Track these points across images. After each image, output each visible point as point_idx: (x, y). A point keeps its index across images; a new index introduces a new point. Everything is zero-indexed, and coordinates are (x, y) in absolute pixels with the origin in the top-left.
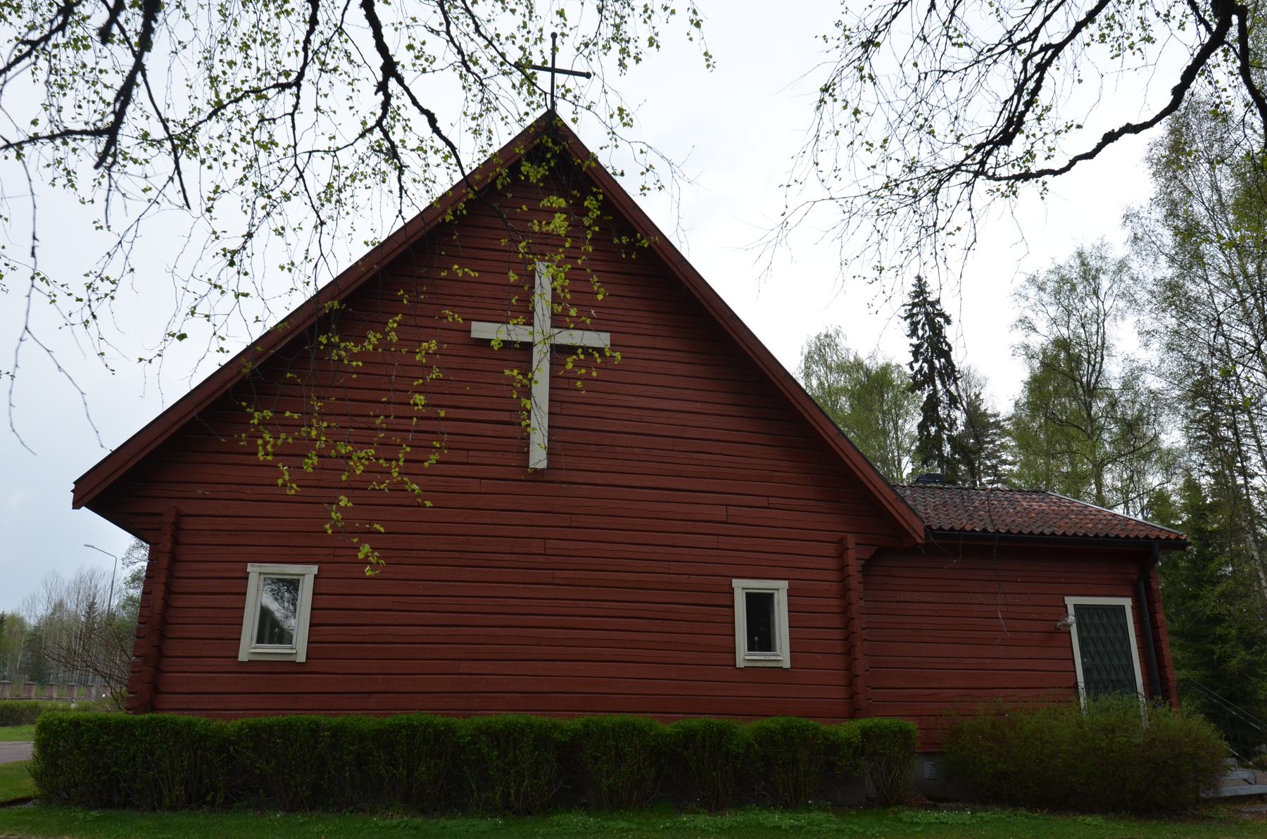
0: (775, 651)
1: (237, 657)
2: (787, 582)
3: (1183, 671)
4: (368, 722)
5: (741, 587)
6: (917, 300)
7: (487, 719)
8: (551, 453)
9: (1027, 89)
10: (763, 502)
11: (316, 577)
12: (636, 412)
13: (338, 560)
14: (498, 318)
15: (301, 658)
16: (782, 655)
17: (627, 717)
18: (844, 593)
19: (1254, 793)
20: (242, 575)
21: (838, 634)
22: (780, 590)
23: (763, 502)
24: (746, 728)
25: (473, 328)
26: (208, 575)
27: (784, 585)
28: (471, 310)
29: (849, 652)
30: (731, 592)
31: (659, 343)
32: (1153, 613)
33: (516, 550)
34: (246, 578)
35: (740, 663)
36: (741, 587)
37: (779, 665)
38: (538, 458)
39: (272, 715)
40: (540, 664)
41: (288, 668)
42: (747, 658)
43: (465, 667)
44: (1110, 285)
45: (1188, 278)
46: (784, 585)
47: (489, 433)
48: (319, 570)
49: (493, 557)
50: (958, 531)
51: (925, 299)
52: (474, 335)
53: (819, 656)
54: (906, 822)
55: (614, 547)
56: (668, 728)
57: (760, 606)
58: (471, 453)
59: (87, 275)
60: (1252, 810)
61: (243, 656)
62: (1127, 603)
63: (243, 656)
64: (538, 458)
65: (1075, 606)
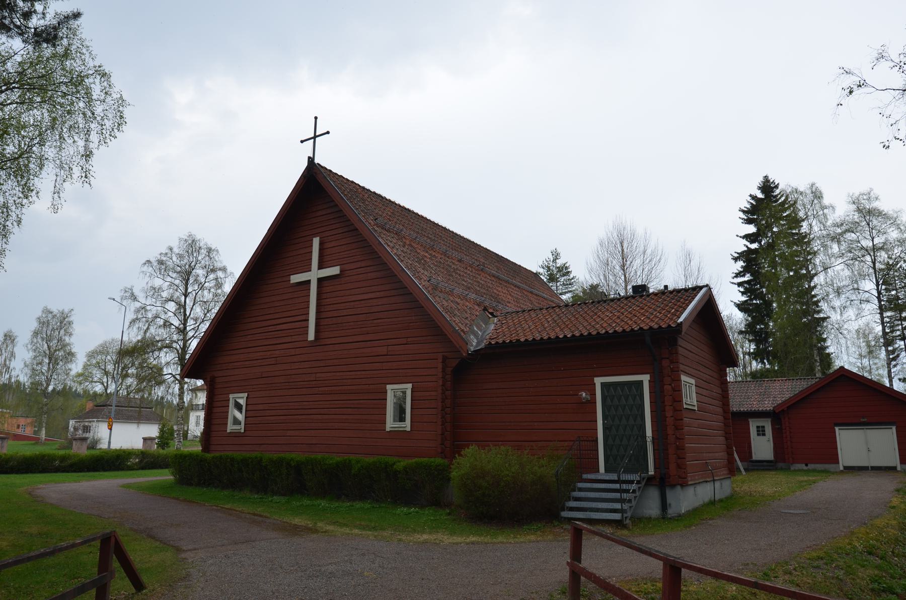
0: (405, 421)
2: (411, 384)
3: (72, 429)
11: (247, 398)
13: (254, 390)
14: (305, 270)
15: (408, 429)
16: (407, 425)
17: (417, 459)
19: (605, 518)
24: (401, 464)
31: (363, 264)
34: (386, 392)
37: (405, 429)
38: (311, 336)
39: (276, 453)
43: (289, 433)
46: (410, 386)
47: (299, 327)
50: (621, 333)
53: (425, 424)
54: (368, 509)
55: (367, 372)
56: (367, 460)
58: (293, 337)
61: (388, 429)
62: (645, 378)
63: (388, 429)
65: (642, 381)
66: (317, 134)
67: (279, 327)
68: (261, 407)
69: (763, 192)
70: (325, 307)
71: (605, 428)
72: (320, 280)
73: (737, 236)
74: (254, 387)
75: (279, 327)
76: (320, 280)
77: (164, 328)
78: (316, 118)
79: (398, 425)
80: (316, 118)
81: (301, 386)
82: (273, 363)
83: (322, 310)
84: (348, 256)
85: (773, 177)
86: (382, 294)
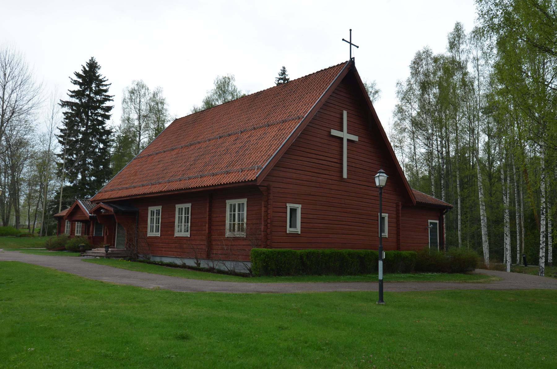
1: (286, 232)
4: (327, 251)
5: (289, 206)
6: (281, 77)
7: (279, 250)
8: (342, 115)
12: (361, 162)
13: (305, 203)
16: (298, 229)
20: (285, 207)
22: (299, 207)
26: (278, 206)
28: (333, 126)
30: (286, 208)
36: (289, 206)
38: (345, 176)
41: (295, 235)
42: (290, 230)
45: (524, 163)
46: (387, 215)
48: (302, 206)
49: (334, 204)
51: (285, 77)
52: (332, 134)
57: (293, 211)
60: (271, 294)
62: (437, 222)
64: (345, 176)
72: (341, 139)
76: (341, 139)
78: (351, 30)
80: (351, 30)
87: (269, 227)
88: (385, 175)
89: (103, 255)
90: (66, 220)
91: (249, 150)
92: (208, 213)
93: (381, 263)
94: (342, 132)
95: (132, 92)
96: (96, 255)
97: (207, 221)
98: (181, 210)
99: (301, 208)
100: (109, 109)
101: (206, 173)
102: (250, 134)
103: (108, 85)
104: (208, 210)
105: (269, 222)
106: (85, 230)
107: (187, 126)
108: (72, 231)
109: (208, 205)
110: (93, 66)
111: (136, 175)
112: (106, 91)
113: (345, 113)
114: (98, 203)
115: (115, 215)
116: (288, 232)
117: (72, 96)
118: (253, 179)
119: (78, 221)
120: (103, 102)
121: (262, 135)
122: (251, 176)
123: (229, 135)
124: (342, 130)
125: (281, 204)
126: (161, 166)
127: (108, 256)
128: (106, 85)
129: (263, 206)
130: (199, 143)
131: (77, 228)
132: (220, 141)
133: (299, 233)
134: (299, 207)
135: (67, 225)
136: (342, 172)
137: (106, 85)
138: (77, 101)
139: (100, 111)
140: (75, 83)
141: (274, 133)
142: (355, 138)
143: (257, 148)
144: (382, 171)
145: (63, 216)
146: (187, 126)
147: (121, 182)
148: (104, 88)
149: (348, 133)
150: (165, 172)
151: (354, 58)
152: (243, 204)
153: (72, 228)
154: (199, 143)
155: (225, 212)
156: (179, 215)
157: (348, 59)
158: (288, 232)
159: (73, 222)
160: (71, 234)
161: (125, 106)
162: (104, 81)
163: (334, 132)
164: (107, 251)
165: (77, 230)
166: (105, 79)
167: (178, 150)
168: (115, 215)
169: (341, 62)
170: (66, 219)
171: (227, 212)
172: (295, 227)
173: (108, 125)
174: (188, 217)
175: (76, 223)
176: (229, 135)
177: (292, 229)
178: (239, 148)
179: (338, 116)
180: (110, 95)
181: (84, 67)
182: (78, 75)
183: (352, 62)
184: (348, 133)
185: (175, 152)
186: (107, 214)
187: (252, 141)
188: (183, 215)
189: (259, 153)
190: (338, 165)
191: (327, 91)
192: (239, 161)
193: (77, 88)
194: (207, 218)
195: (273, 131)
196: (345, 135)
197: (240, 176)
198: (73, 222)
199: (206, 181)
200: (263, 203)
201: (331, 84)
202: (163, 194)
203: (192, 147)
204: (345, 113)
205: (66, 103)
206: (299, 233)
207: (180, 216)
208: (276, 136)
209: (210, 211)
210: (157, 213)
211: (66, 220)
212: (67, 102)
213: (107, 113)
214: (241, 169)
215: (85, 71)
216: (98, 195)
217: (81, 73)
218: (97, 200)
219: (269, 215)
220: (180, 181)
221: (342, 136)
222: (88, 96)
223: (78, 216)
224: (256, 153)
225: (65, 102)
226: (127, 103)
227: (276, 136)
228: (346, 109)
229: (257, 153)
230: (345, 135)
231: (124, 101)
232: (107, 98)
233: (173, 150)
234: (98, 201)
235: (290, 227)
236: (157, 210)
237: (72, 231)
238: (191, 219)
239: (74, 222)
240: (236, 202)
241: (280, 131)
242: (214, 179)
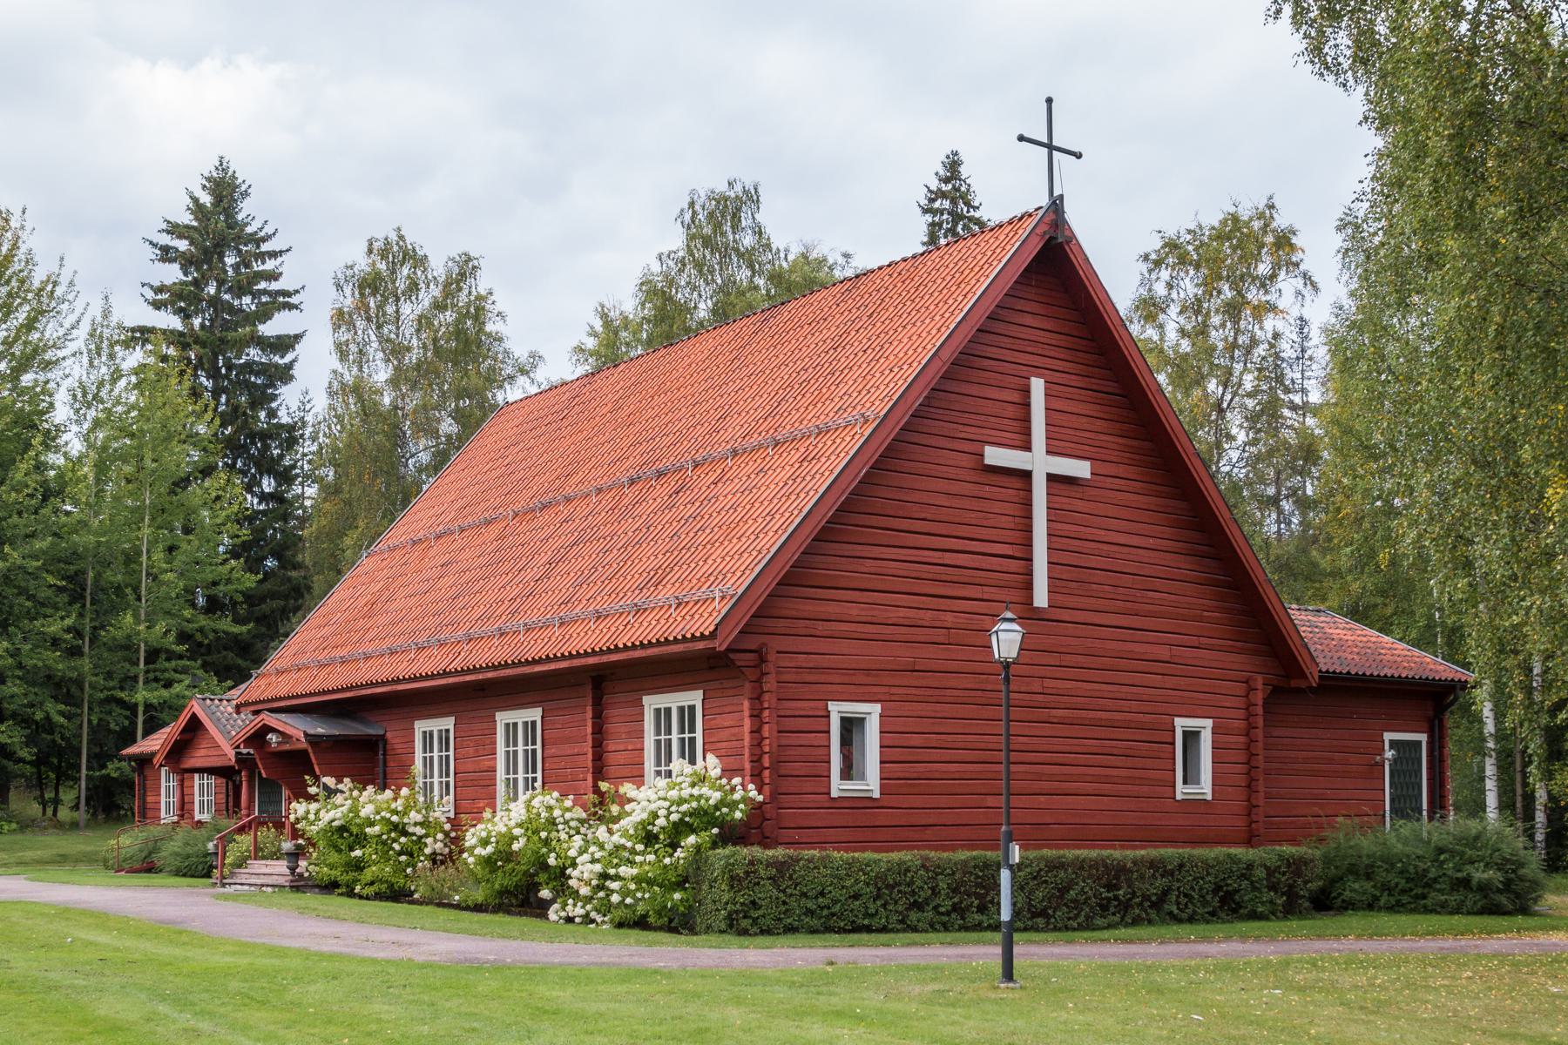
1: (829, 794)
8: (1026, 391)
9: (12, 478)
10: (1194, 640)
12: (1105, 547)
16: (871, 783)
18: (1248, 731)
20: (824, 714)
21: (1241, 768)
22: (872, 712)
23: (1194, 640)
25: (986, 454)
26: (797, 713)
27: (1209, 723)
29: (1250, 786)
32: (1442, 747)
33: (1023, 689)
35: (1179, 797)
40: (1042, 798)
44: (921, 249)
52: (988, 461)
53: (1230, 789)
59: (1361, 182)
62: (1423, 738)
66: (1045, 140)
67: (949, 558)
68: (916, 740)
69: (212, 192)
70: (1012, 526)
71: (1392, 800)
72: (1026, 475)
73: (75, 272)
74: (894, 690)
75: (949, 558)
76: (1026, 475)
77: (48, 365)
78: (1049, 101)
79: (852, 787)
80: (1049, 101)
81: (951, 700)
82: (941, 639)
83: (1018, 534)
84: (1089, 442)
85: (243, 172)
86: (1135, 541)
87: (767, 781)
88: (1015, 627)
89: (281, 881)
90: (163, 770)
91: (708, 531)
92: (590, 738)
93: (1005, 876)
94: (1027, 454)
95: (370, 284)
96: (259, 881)
97: (590, 764)
98: (663, 716)
99: (881, 716)
100: (285, 344)
101: (577, 610)
102: (719, 471)
103: (281, 252)
104: (589, 730)
105: (767, 765)
106: (227, 802)
107: (538, 432)
108: (184, 808)
109: (589, 714)
110: (225, 190)
111: (369, 615)
112: (273, 276)
113: (1038, 386)
114: (256, 713)
115: (310, 750)
116: (834, 794)
117: (157, 305)
118: (707, 633)
119: (201, 770)
120: (265, 314)
121: (753, 476)
122: (703, 622)
123: (660, 474)
124: (1027, 447)
125: (812, 704)
126: (448, 581)
127: (300, 884)
128: (274, 255)
129: (747, 713)
130: (568, 500)
131: (201, 794)
132: (630, 494)
133: (876, 795)
134: (872, 712)
135: (167, 784)
136: (1029, 586)
137: (274, 255)
138: (174, 322)
139: (254, 353)
140: (166, 254)
141: (788, 471)
142: (1080, 469)
143: (733, 526)
144: (1009, 615)
145: (153, 754)
146: (538, 432)
147: (325, 638)
148: (270, 265)
149: (1049, 452)
150: (461, 603)
151: (1061, 197)
152: (692, 708)
153: (183, 795)
154: (568, 500)
155: (640, 735)
156: (658, 733)
157: (1044, 201)
158: (834, 794)
159: (184, 774)
160: (182, 816)
161: (344, 336)
162: (264, 240)
163: (995, 456)
164: (293, 869)
165: (202, 803)
166: (269, 230)
167: (504, 524)
168: (310, 750)
169: (1024, 211)
170: (161, 765)
171: (646, 735)
172: (862, 777)
173: (287, 401)
174: (534, 752)
175: (196, 776)
176: (660, 474)
177: (1190, 789)
178: (683, 522)
179: (1015, 397)
180: (291, 289)
181: (195, 200)
182: (174, 229)
183: (1056, 205)
184: (1049, 452)
185: (495, 530)
186: (287, 747)
187: (721, 498)
188: (675, 736)
189: (735, 541)
190: (1014, 565)
191: (960, 322)
192: (676, 568)
193: (172, 274)
194: (590, 756)
195: (784, 465)
196: (1040, 462)
197: (671, 620)
198: (184, 774)
199: (575, 635)
200: (746, 704)
201: (979, 293)
202: (451, 680)
203: (547, 516)
204: (1038, 386)
205: (138, 335)
206: (876, 795)
207: (663, 737)
208: (790, 482)
209: (599, 731)
210: (440, 738)
211: (163, 770)
212: (144, 330)
213: (277, 359)
214: (677, 598)
215: (198, 208)
216: (261, 685)
217: (187, 219)
218: (253, 703)
219: (767, 742)
220: (502, 635)
221: (1027, 467)
222: (215, 302)
223: (200, 757)
224: (726, 543)
225: (133, 330)
226: (351, 325)
227: (790, 482)
228: (1038, 370)
229: (730, 541)
230: (1040, 462)
231: (341, 319)
232: (282, 302)
233: (488, 523)
234: (257, 707)
235: (1185, 782)
236: (440, 731)
237: (184, 808)
238: (543, 758)
239: (186, 775)
240: (675, 701)
241: (806, 464)
242: (598, 632)
